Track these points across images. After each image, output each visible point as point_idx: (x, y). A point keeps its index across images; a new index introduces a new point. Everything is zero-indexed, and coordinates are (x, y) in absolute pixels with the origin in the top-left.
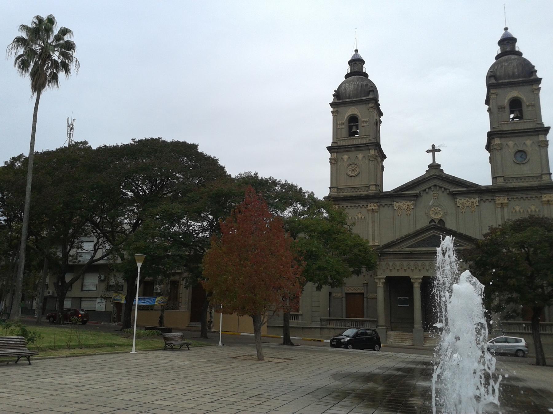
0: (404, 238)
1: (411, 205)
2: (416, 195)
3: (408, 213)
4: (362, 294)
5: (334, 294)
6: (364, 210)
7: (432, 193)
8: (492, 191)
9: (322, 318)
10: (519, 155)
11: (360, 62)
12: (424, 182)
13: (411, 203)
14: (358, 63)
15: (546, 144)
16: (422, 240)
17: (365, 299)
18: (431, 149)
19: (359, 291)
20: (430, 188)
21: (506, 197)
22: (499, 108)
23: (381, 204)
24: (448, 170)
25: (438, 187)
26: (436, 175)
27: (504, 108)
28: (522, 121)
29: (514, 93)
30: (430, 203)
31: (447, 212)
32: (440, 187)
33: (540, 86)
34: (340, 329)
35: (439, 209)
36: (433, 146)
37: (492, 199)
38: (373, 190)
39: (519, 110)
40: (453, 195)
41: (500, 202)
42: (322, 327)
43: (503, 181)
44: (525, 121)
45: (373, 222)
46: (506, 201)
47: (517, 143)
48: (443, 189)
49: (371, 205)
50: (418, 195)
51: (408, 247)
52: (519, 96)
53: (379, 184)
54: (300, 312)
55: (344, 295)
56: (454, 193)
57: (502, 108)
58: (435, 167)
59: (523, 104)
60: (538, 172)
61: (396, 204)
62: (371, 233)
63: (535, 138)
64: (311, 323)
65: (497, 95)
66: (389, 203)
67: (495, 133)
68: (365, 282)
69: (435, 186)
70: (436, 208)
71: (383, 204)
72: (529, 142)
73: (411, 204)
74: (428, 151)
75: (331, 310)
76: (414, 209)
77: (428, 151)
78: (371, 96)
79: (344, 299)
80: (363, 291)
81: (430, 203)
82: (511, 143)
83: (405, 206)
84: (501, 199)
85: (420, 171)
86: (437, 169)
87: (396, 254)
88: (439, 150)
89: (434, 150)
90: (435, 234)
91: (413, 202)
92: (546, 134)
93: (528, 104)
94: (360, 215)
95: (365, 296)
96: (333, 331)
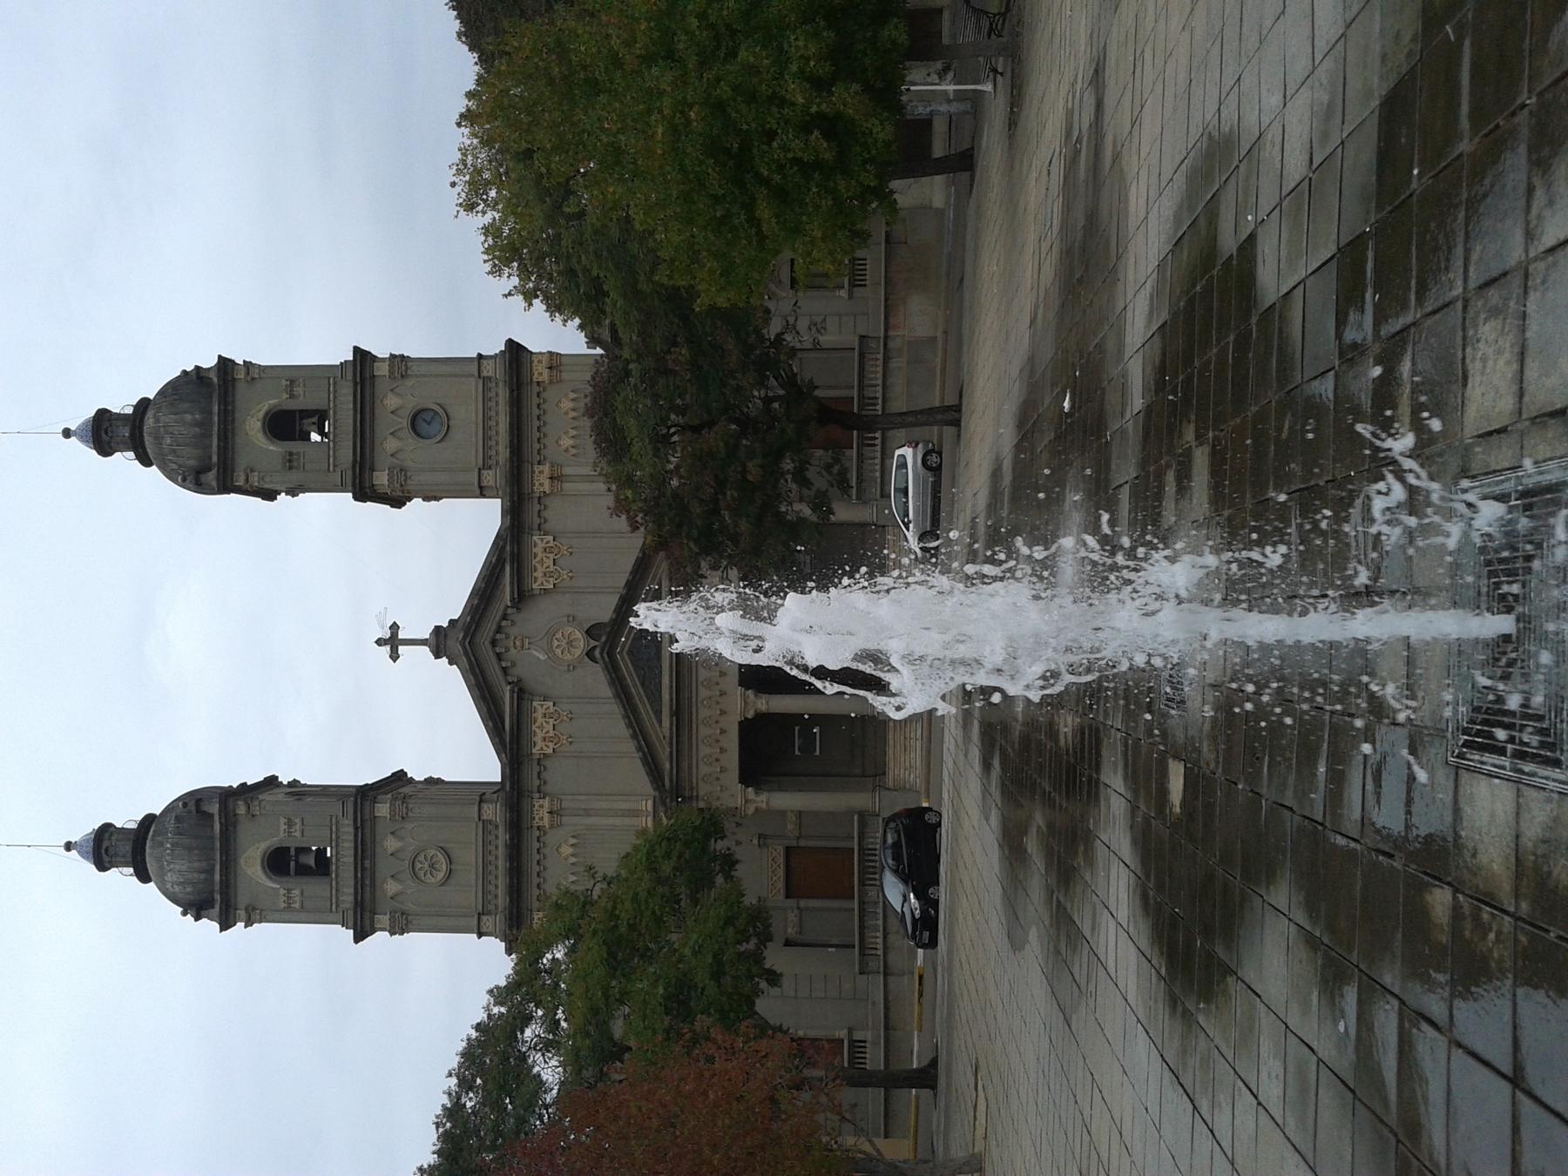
0: (635, 731)
1: (545, 707)
2: (515, 695)
3: (565, 718)
4: (788, 850)
5: (789, 930)
6: (551, 838)
7: (513, 651)
8: (516, 499)
9: (857, 970)
10: (423, 427)
11: (107, 835)
12: (482, 672)
13: (539, 707)
14: (106, 844)
15: (399, 363)
16: (643, 685)
17: (803, 843)
18: (388, 648)
19: (781, 860)
20: (499, 657)
21: (535, 467)
22: (290, 468)
23: (535, 789)
24: (452, 605)
25: (498, 636)
26: (464, 638)
27: (291, 454)
28: (331, 412)
29: (252, 427)
30: (542, 657)
31: (568, 616)
32: (499, 630)
33: (242, 363)
34: (885, 916)
35: (559, 635)
36: (380, 642)
37: (539, 503)
38: (494, 812)
39: (301, 419)
40: (522, 597)
41: (547, 483)
42: (882, 969)
43: (490, 472)
44: (331, 406)
45: (587, 813)
46: (546, 468)
47: (392, 430)
48: (504, 623)
49: (537, 817)
50: (516, 690)
51: (660, 722)
52: (261, 414)
53: (477, 792)
54: (843, 1034)
55: (792, 902)
56: (516, 596)
57: (290, 461)
58: (442, 638)
59: (285, 408)
60: (472, 387)
61: (538, 747)
62: (618, 821)
63: (382, 387)
64: (874, 1003)
65: (252, 471)
66: (536, 769)
67: (357, 481)
68: (755, 841)
69: (494, 643)
70: (556, 643)
71: (537, 782)
72: (391, 401)
73: (540, 708)
74: (394, 656)
75: (835, 941)
76: (556, 700)
77: (394, 656)
78: (214, 809)
79: (803, 903)
80: (781, 849)
81: (542, 657)
82: (391, 445)
83: (545, 724)
84: (541, 480)
85: (449, 681)
86: (446, 635)
87: (678, 756)
88: (395, 627)
89: (393, 642)
90: (626, 649)
91: (535, 703)
92: (374, 358)
93: (285, 396)
94: (566, 850)
95: (794, 843)
96: (892, 938)
